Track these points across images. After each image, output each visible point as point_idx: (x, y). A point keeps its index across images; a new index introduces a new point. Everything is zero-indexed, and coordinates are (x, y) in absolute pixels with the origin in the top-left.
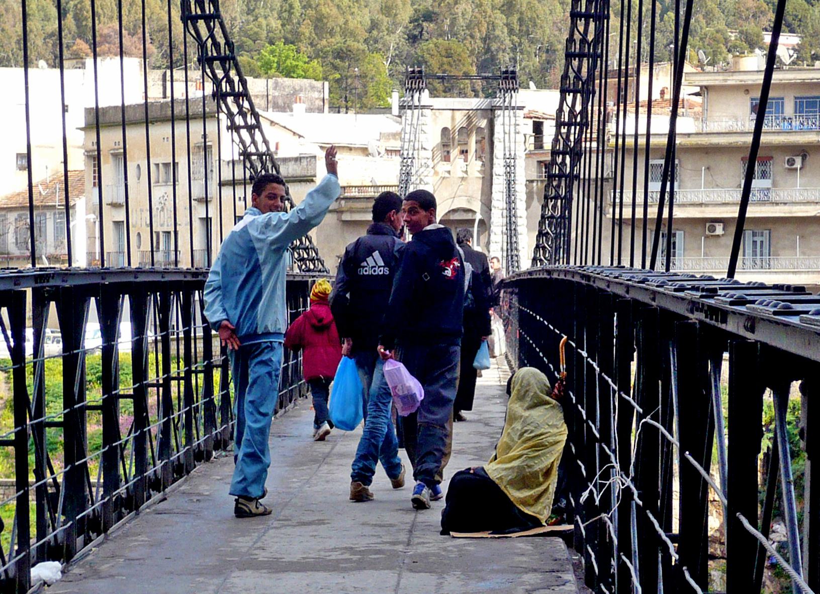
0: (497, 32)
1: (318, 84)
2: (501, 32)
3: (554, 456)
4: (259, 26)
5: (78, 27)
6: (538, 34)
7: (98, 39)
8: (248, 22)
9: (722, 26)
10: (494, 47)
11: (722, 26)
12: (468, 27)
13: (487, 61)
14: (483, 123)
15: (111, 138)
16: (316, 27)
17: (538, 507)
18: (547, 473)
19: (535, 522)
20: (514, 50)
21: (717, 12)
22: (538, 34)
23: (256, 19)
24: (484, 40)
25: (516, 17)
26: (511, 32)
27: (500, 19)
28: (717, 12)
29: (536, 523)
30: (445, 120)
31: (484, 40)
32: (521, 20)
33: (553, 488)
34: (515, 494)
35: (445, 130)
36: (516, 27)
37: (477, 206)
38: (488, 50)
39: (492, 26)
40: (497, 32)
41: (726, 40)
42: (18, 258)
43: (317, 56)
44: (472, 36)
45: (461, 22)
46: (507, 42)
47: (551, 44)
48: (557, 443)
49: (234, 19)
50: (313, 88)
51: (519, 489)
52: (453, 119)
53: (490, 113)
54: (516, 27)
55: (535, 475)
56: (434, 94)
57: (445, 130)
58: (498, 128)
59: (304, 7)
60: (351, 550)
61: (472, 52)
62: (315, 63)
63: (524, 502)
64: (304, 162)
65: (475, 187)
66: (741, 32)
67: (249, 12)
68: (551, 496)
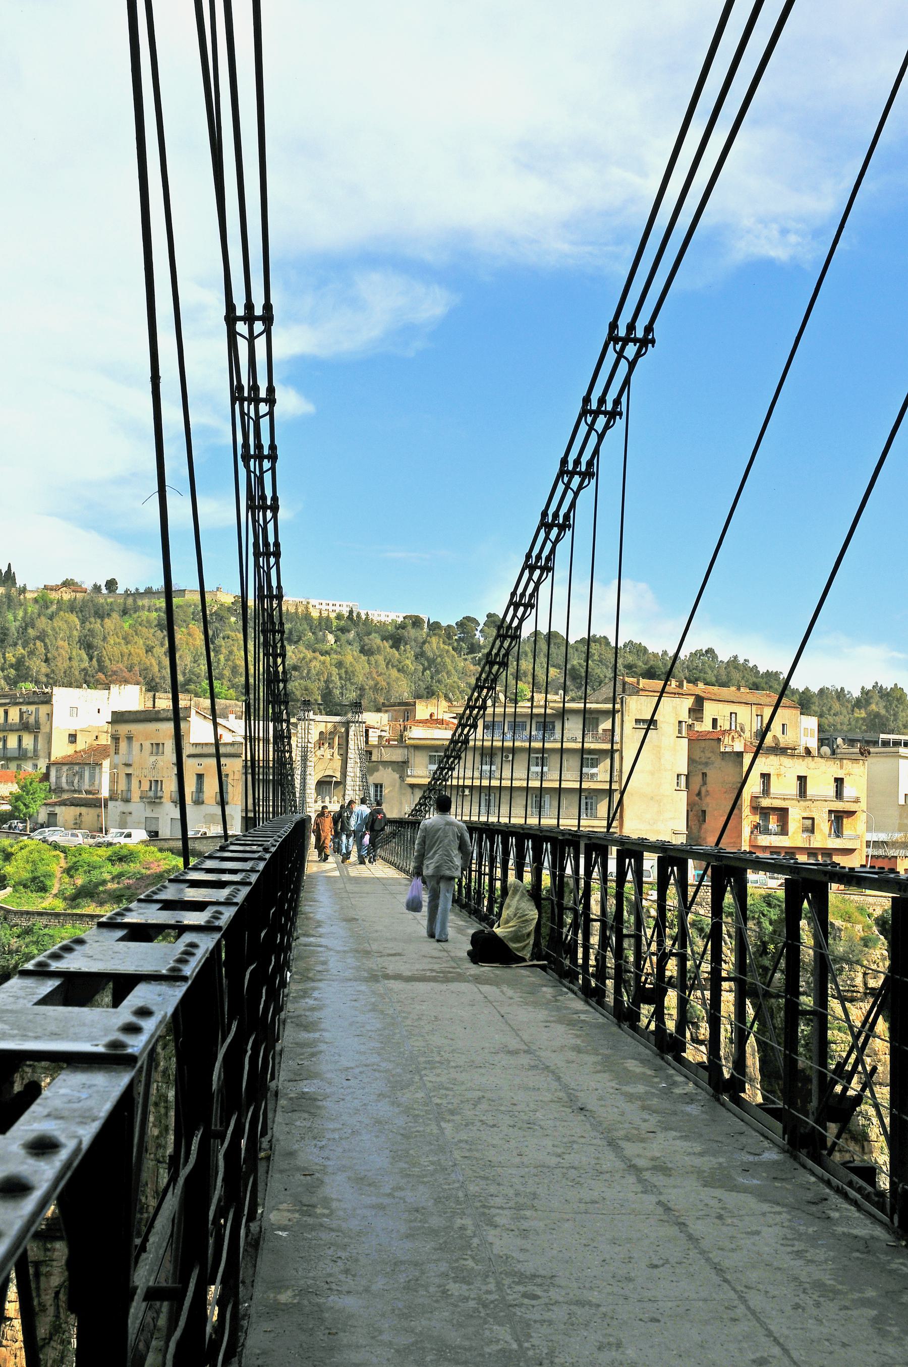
0: (333, 678)
1: (240, 703)
2: (335, 678)
3: (532, 927)
4: (201, 670)
5: (99, 665)
6: (355, 680)
7: (180, 678)
8: (194, 667)
9: (456, 679)
10: (331, 686)
11: (456, 679)
12: (317, 675)
13: (327, 695)
14: (343, 730)
15: (123, 729)
16: (232, 672)
17: (525, 953)
18: (529, 935)
19: (523, 960)
20: (342, 687)
21: (453, 671)
22: (355, 680)
23: (199, 665)
24: (325, 682)
25: (343, 670)
26: (341, 678)
27: (335, 671)
28: (453, 671)
29: (524, 960)
30: (322, 727)
31: (325, 682)
32: (346, 672)
33: (532, 942)
34: (513, 945)
35: (321, 733)
36: (344, 676)
37: (338, 775)
38: (327, 687)
39: (330, 675)
40: (333, 678)
41: (459, 687)
42: (68, 791)
43: (233, 687)
44: (319, 680)
45: (313, 672)
46: (338, 684)
47: (362, 685)
48: (533, 919)
49: (186, 665)
50: (236, 705)
51: (515, 943)
52: (326, 727)
53: (347, 724)
54: (344, 676)
55: (523, 936)
56: (315, 714)
57: (321, 733)
58: (351, 733)
59: (226, 660)
60: (432, 970)
61: (319, 688)
62: (231, 691)
63: (518, 949)
64: (236, 746)
65: (337, 763)
66: (467, 683)
67: (195, 662)
68: (530, 948)
